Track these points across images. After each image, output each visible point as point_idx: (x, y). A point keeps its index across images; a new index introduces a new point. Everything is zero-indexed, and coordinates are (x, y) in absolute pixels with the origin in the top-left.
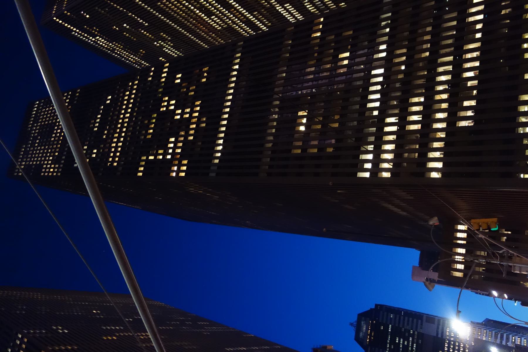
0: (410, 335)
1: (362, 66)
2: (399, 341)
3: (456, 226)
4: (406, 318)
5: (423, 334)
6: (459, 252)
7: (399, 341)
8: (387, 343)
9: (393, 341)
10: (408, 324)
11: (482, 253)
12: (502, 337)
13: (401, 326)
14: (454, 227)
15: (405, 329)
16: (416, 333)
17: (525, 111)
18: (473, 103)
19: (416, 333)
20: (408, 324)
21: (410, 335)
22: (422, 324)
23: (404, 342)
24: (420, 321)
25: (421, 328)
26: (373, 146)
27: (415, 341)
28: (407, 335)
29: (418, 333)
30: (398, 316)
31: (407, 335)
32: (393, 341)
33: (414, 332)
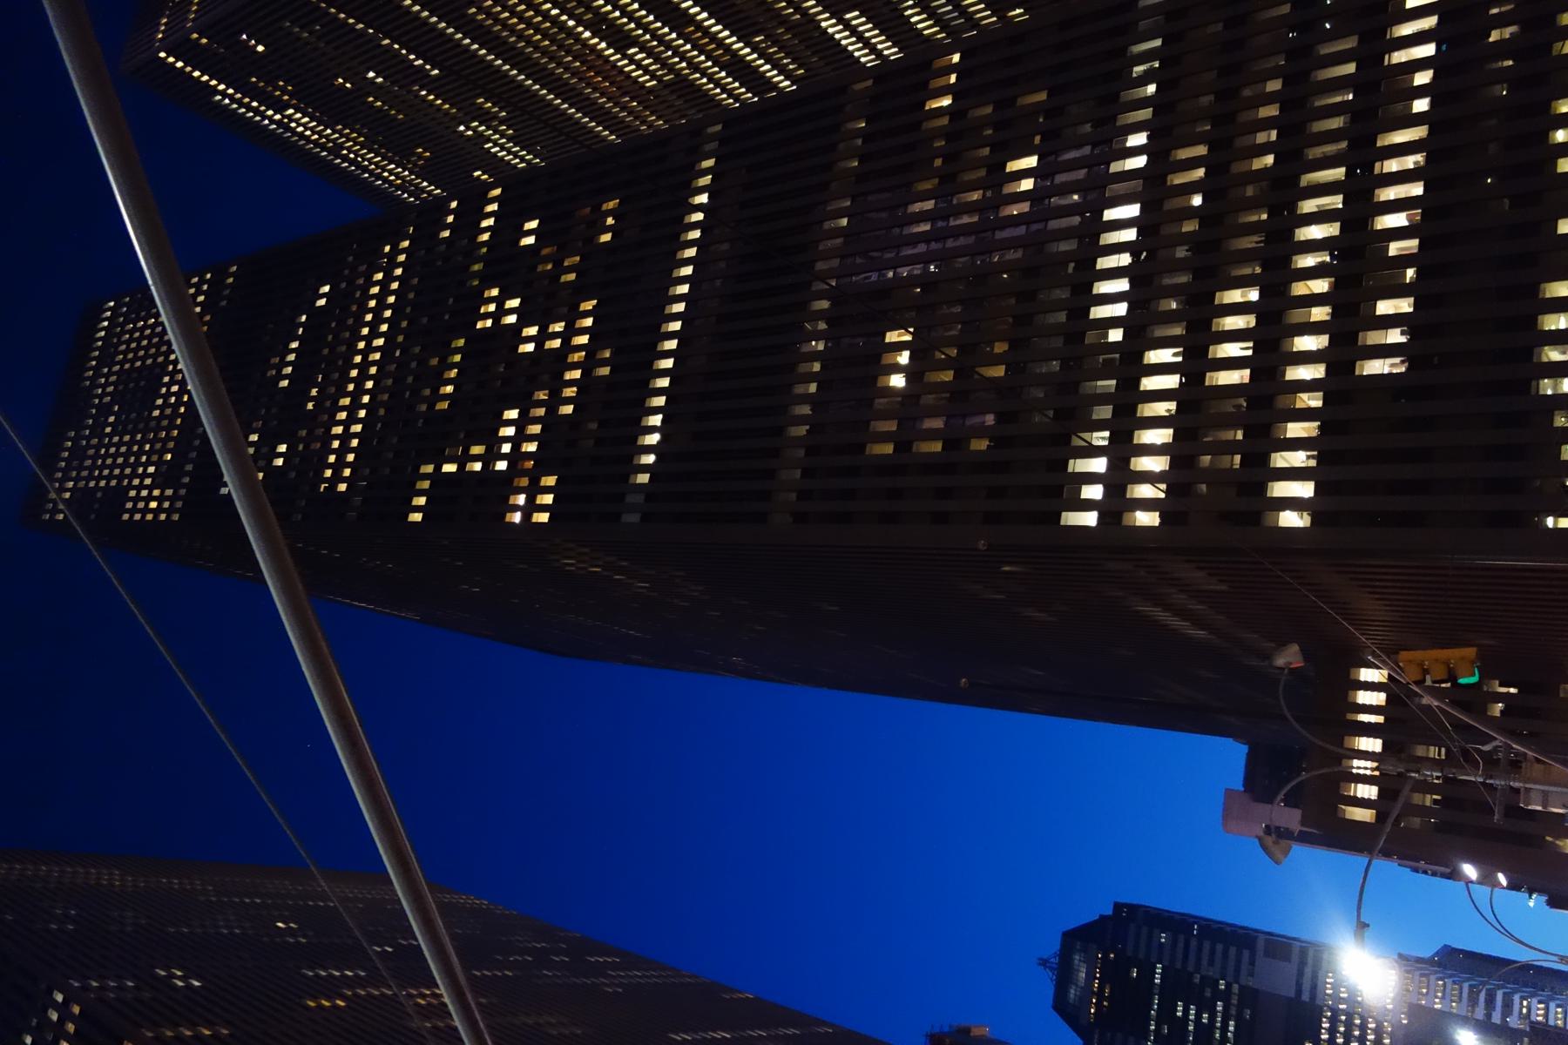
0: (1218, 995)
2: (1186, 1011)
3: (1353, 670)
4: (1207, 945)
5: (1256, 991)
6: (1363, 747)
7: (1186, 1011)
8: (1148, 1019)
9: (1167, 1012)
10: (1211, 963)
11: (1433, 752)
13: (1190, 969)
14: (1348, 674)
15: (1202, 978)
16: (1235, 988)
17: (1558, 331)
18: (1405, 306)
19: (1235, 988)
20: (1211, 963)
21: (1218, 995)
22: (1252, 963)
23: (1198, 1016)
24: (1246, 953)
25: (1251, 974)
26: (1107, 434)
27: (1233, 1012)
28: (1208, 994)
29: (1242, 988)
30: (1181, 938)
31: (1208, 994)
32: (1167, 1012)
33: (1228, 985)
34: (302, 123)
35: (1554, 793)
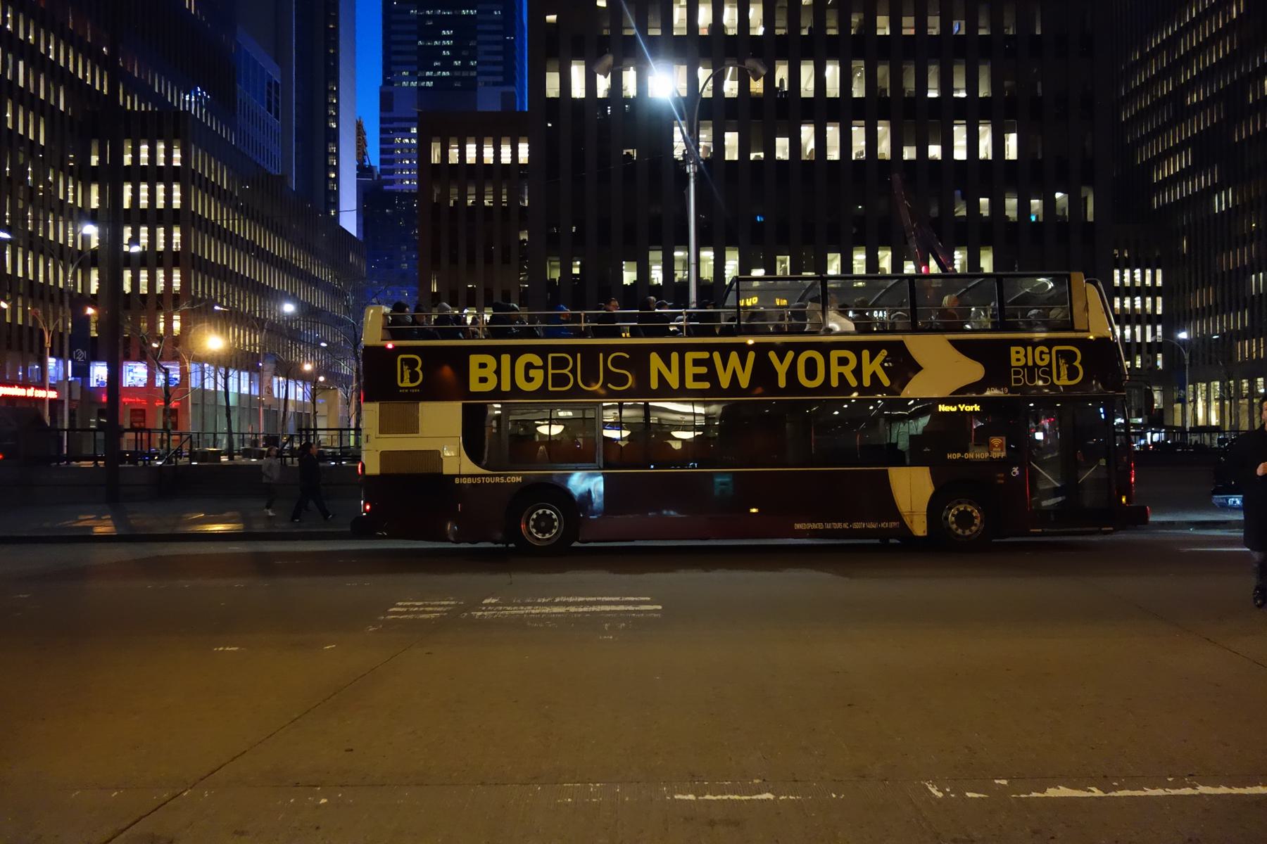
0: (465, 61)
1: (1183, 335)
2: (447, 38)
3: (456, 139)
4: (500, 48)
5: (476, 89)
6: (485, 150)
7: (447, 38)
8: (435, 9)
9: (443, 22)
10: (487, 53)
11: (504, 198)
12: (56, 318)
13: (480, 37)
14: (487, 136)
15: (474, 48)
16: (474, 74)
17: (714, 260)
18: (732, 154)
19: (474, 74)
20: (487, 53)
21: (465, 61)
22: (495, 84)
23: (446, 48)
24: (500, 79)
25: (486, 84)
26: (963, 32)
27: (457, 74)
28: (464, 53)
29: (475, 78)
30: (501, 27)
31: (464, 53)
32: (443, 22)
33: (473, 68)
34: (1063, 792)
35: (3, 404)
